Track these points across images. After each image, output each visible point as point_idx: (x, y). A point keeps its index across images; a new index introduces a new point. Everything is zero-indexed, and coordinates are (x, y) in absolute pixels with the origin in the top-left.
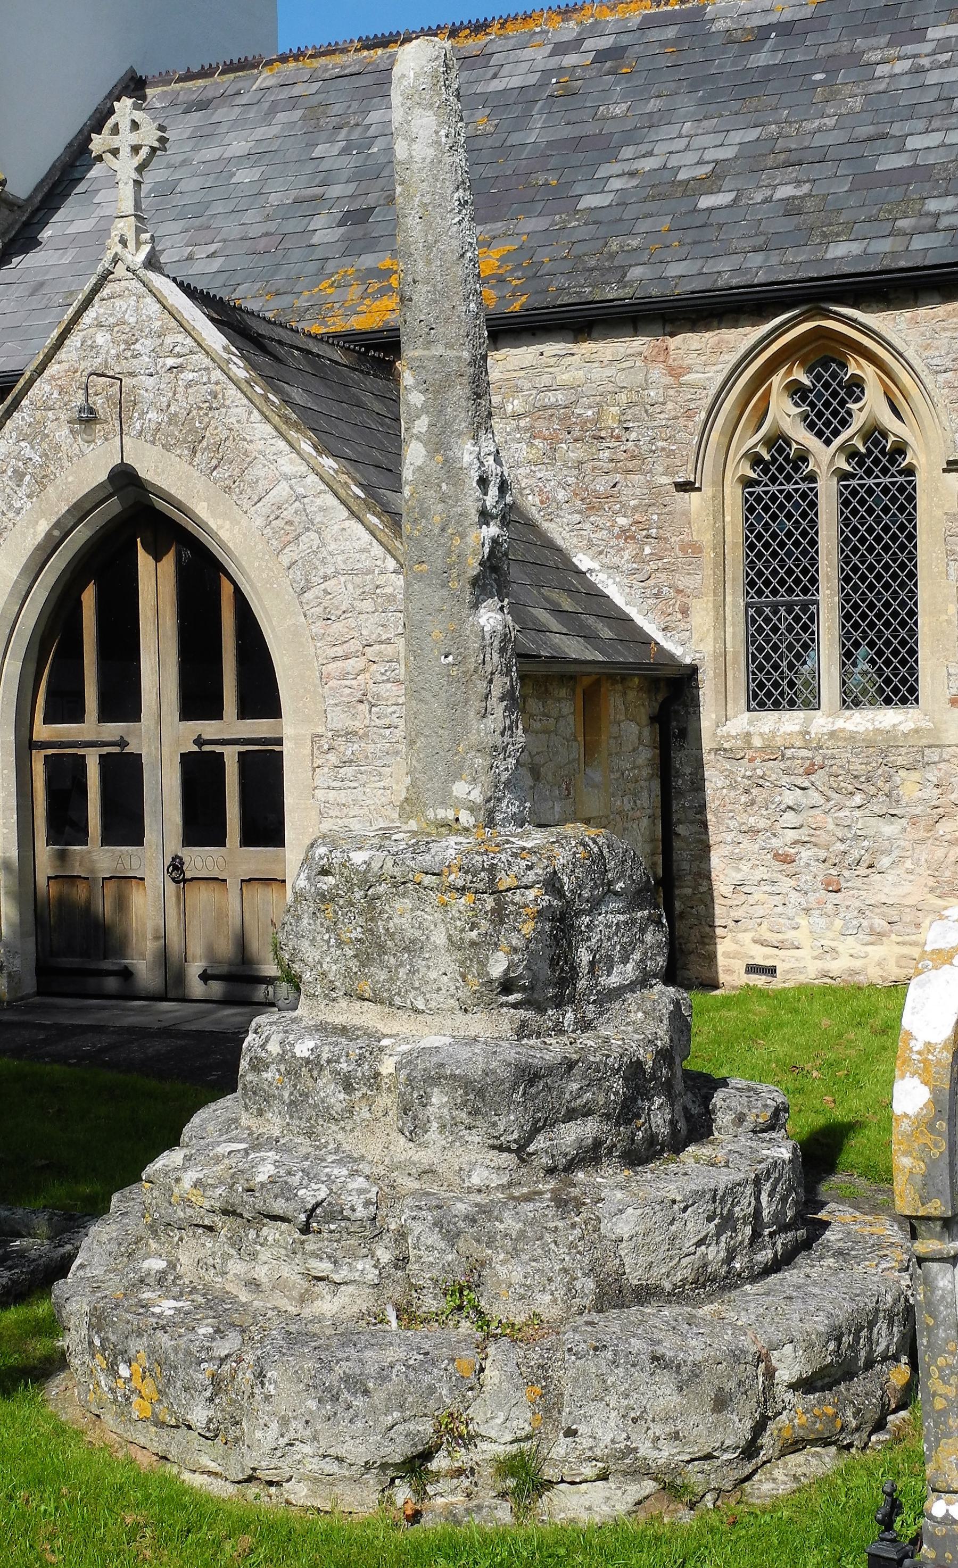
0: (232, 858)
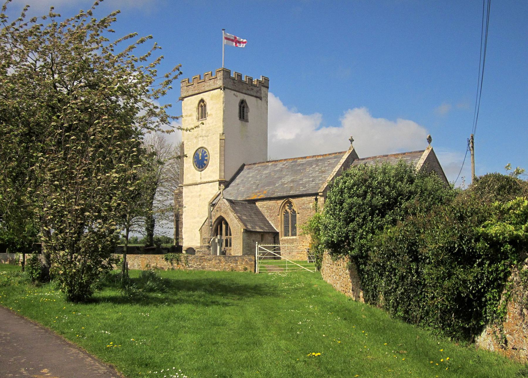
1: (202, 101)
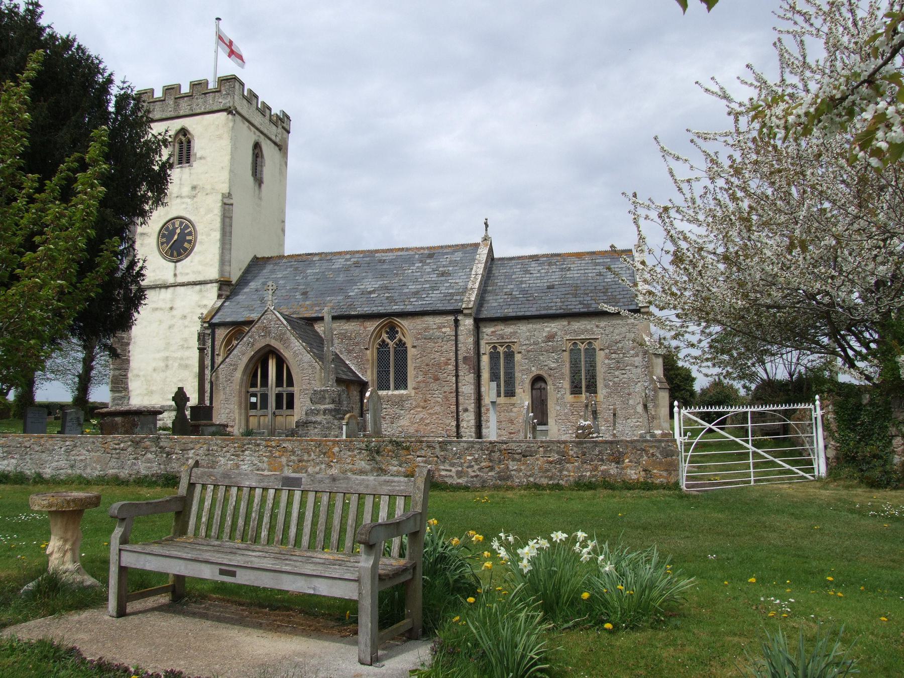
0: (285, 411)
1: (184, 131)
